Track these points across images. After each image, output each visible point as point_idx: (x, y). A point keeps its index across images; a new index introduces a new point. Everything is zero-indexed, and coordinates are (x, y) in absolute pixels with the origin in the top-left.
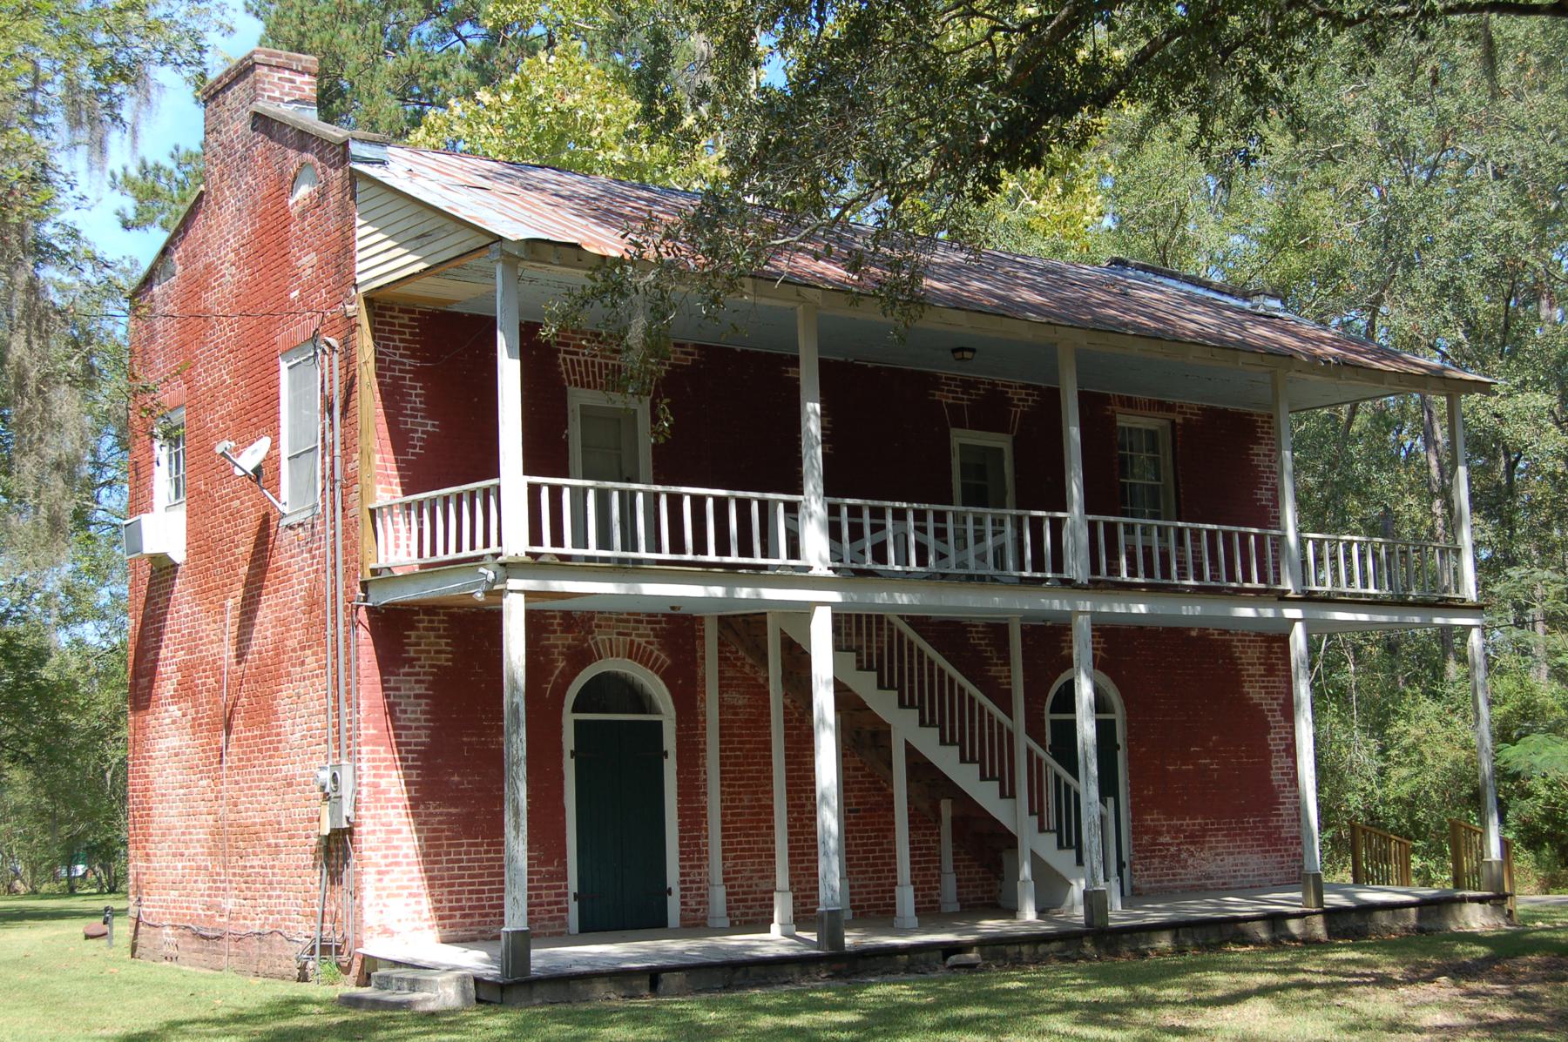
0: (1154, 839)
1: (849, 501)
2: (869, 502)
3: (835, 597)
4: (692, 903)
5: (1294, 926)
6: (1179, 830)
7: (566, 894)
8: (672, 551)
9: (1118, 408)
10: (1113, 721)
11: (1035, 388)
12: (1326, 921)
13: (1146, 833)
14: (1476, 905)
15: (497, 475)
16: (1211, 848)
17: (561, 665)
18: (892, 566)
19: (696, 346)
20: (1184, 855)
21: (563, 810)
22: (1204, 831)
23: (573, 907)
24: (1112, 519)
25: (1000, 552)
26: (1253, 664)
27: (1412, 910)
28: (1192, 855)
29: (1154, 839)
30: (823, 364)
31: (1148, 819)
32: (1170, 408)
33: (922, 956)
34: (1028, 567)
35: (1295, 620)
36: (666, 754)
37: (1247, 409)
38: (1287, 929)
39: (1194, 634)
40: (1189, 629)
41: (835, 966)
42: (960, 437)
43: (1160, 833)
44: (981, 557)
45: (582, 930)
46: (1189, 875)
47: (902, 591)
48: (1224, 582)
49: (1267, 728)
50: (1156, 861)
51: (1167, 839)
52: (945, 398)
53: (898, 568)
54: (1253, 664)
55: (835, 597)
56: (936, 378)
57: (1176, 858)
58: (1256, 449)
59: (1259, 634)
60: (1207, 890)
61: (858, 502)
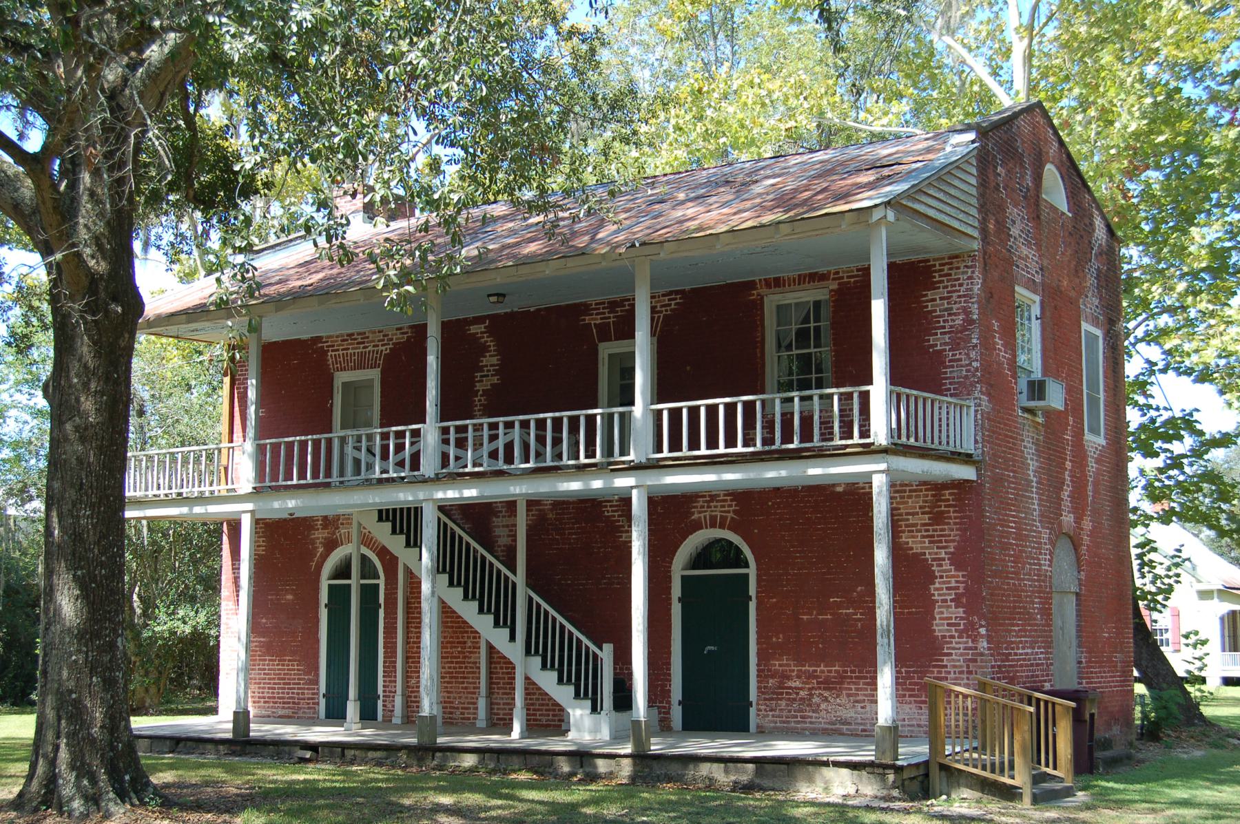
0: (781, 683)
1: (394, 429)
2: (501, 419)
3: (249, 506)
4: (389, 706)
5: (602, 766)
6: (811, 676)
7: (318, 694)
8: (708, 448)
9: (764, 291)
10: (747, 575)
11: (677, 292)
12: (635, 765)
13: (772, 677)
14: (845, 772)
15: (871, 383)
16: (849, 695)
17: (321, 550)
18: (566, 461)
19: (411, 327)
20: (816, 700)
21: (318, 641)
22: (842, 678)
23: (323, 702)
24: (557, 414)
25: (509, 447)
26: (913, 514)
27: (751, 766)
28: (826, 699)
29: (781, 683)
30: (891, 266)
31: (776, 665)
32: (823, 277)
33: (287, 749)
34: (796, 439)
35: (632, 487)
36: (680, 600)
37: (921, 257)
38: (595, 767)
39: (840, 489)
40: (834, 485)
41: (233, 748)
42: (341, 378)
43: (789, 678)
44: (401, 464)
45: (328, 717)
46: (822, 719)
47: (291, 498)
48: (566, 461)
49: (931, 578)
50: (783, 703)
51: (798, 684)
52: (594, 320)
53: (572, 462)
54: (913, 514)
55: (249, 506)
56: (753, 282)
57: (807, 701)
58: (930, 294)
59: (925, 483)
60: (843, 734)
61: (318, 436)
